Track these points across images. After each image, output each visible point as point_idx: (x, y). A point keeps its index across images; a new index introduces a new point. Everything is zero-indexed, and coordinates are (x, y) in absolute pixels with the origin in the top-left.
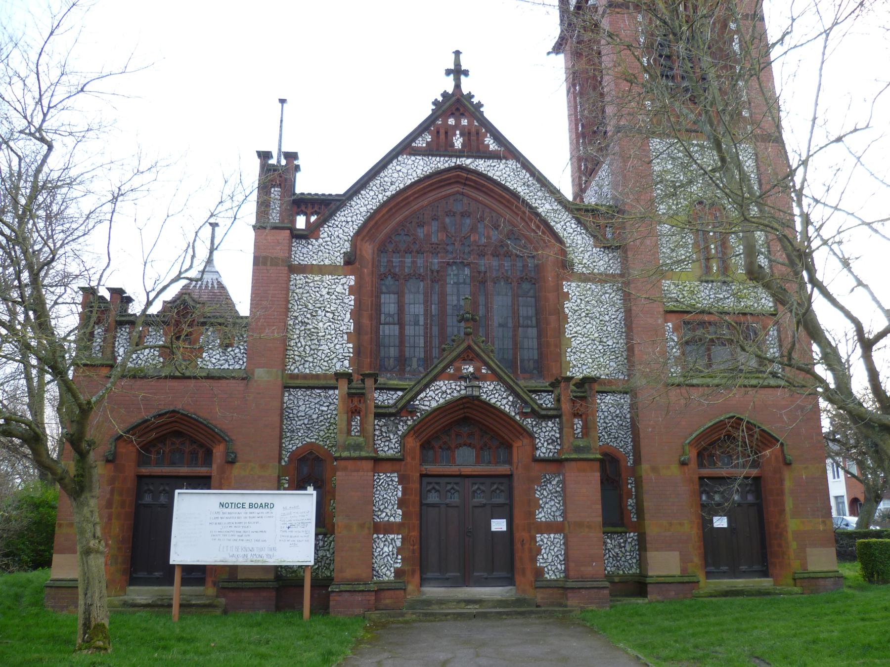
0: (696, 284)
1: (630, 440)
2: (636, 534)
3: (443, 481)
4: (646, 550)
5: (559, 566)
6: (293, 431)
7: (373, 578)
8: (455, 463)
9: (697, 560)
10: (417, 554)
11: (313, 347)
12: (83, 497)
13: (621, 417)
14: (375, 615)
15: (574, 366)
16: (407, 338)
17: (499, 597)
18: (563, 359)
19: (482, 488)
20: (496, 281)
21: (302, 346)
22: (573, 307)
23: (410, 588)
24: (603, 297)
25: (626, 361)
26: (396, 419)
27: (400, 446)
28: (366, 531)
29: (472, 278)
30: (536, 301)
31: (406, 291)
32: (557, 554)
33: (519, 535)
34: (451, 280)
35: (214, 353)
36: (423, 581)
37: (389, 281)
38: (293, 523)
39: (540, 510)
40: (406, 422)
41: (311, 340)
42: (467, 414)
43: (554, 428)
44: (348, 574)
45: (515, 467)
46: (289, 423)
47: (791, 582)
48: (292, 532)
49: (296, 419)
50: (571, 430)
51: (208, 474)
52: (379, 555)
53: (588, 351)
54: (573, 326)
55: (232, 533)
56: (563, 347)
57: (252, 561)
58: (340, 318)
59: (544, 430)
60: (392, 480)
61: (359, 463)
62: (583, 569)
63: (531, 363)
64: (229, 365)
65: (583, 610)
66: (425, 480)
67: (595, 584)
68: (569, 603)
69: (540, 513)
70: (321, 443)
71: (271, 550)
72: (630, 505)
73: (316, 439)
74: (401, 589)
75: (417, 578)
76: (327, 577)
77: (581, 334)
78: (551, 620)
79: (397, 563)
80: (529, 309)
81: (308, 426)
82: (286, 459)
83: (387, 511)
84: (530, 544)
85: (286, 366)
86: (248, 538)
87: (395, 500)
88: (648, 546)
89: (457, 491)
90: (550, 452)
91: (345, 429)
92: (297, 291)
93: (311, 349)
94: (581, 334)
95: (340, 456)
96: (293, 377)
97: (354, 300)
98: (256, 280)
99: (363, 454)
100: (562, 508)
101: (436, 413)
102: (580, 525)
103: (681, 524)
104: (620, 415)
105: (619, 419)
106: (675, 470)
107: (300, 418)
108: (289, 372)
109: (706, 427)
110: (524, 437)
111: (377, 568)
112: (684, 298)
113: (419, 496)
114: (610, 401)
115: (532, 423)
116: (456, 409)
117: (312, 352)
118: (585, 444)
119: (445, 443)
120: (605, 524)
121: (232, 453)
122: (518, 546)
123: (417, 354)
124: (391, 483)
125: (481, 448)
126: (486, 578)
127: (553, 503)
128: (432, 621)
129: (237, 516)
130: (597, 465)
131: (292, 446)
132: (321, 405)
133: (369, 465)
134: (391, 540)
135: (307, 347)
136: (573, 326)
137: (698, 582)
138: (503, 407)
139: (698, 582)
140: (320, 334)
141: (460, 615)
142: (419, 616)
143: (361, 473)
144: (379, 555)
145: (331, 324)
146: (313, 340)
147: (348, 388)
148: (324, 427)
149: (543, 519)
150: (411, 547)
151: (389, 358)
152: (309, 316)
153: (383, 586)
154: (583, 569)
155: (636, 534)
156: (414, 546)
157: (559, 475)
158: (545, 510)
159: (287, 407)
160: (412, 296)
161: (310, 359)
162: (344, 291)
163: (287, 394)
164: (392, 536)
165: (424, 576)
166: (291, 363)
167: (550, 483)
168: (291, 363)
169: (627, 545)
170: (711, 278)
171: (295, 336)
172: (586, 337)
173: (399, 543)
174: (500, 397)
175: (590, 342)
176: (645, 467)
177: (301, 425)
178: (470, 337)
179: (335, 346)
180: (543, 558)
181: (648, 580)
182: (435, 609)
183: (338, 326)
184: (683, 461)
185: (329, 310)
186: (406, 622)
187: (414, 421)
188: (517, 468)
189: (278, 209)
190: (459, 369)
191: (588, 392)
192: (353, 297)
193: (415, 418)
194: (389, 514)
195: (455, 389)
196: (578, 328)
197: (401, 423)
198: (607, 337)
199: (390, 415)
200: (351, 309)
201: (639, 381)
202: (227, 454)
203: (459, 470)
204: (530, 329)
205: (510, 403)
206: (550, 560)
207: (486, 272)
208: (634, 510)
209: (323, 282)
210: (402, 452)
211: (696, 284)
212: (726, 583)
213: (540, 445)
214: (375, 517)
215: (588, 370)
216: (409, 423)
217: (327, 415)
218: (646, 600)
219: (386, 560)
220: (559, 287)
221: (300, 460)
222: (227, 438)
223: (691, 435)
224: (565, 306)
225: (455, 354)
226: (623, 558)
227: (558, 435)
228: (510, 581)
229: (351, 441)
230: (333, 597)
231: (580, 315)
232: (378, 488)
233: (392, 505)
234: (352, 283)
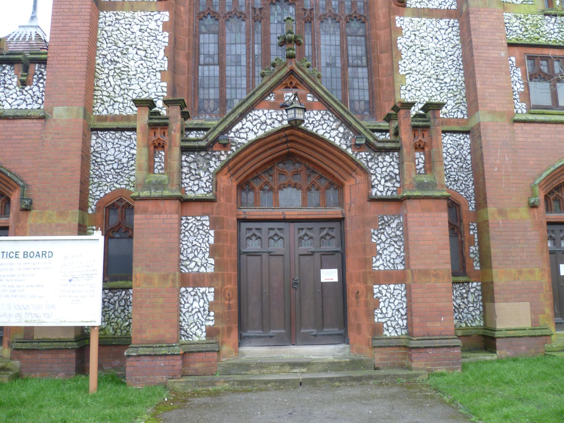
0: (539, 17)
1: (471, 183)
2: (480, 284)
3: (265, 226)
4: (493, 301)
5: (400, 322)
6: (101, 177)
7: (181, 338)
8: (278, 205)
9: (548, 311)
10: (235, 310)
11: (123, 87)
13: (461, 159)
14: (179, 384)
16: (228, 79)
17: (331, 358)
19: (310, 234)
20: (323, 19)
21: (111, 86)
22: (407, 43)
23: (225, 349)
24: (439, 33)
25: (465, 99)
26: (207, 154)
27: (212, 185)
28: (169, 284)
29: (297, 16)
30: (366, 40)
31: (227, 30)
32: (397, 307)
33: (351, 286)
34: (274, 19)
35: (11, 92)
36: (242, 340)
37: (209, 21)
39: (378, 257)
40: (219, 158)
41: (121, 80)
42: (291, 150)
43: (393, 163)
44: (149, 334)
45: (347, 209)
46: (97, 168)
49: (104, 163)
50: (412, 164)
51: (6, 225)
52: (188, 311)
53: (424, 88)
54: (407, 62)
57: (27, 322)
58: (152, 56)
59: (381, 165)
60: (203, 225)
61: (161, 204)
62: (429, 324)
63: (362, 103)
64: (27, 105)
65: (431, 374)
66: (244, 226)
67: (444, 343)
68: (414, 365)
69: (377, 260)
72: (473, 253)
73: (126, 185)
74: (214, 351)
75: (235, 335)
77: (416, 71)
78: (395, 390)
79: (209, 320)
80: (359, 48)
82: (93, 207)
83: (197, 260)
84: (366, 297)
85: (94, 107)
87: (205, 247)
88: (496, 296)
89: (282, 238)
90: (388, 190)
91: (145, 164)
92: (107, 28)
93: (121, 89)
94: (416, 71)
95: (139, 196)
96: (101, 118)
97: (169, 37)
98: (56, 7)
99: (166, 193)
100: (403, 254)
101: (254, 147)
102: (425, 273)
103: (531, 272)
104: (460, 156)
105: (459, 160)
106: (524, 213)
107: (109, 162)
108: (97, 114)
109: (557, 166)
110: (357, 174)
111: (186, 327)
112: (527, 31)
113: (236, 242)
114: (449, 142)
115: (366, 158)
116: (279, 142)
117: (122, 92)
118: (429, 179)
119: (267, 183)
120: (454, 274)
121: (27, 199)
122: (351, 299)
123: (239, 96)
124: (201, 227)
125: (309, 189)
126: (315, 336)
127: (392, 249)
128: (248, 391)
130: (444, 203)
132: (131, 148)
133: (175, 205)
135: (116, 87)
136: (407, 62)
137: (550, 335)
138: (332, 139)
139: (550, 335)
140: (131, 73)
141: (283, 382)
142: (233, 385)
143: (164, 216)
144: (188, 311)
145: (143, 62)
146: (124, 79)
147: (150, 119)
148: (134, 172)
149: (382, 268)
150: (227, 302)
151: (209, 100)
152: (119, 54)
153: (193, 348)
154: (429, 324)
155: (480, 284)
156: (230, 300)
157: (399, 217)
158: (383, 256)
159: (94, 151)
160: (233, 36)
161: (120, 99)
162: (157, 28)
163: (94, 137)
164: (202, 290)
165: (244, 334)
166: (99, 104)
167: (389, 225)
168: (99, 104)
169: (470, 296)
170: (553, 12)
171: (104, 76)
172: (422, 75)
173: (211, 298)
174: (329, 128)
175: (426, 79)
176: (491, 209)
177: (110, 170)
178: (293, 60)
179: (147, 85)
180: (382, 313)
181: (497, 334)
182: (255, 375)
183: (150, 64)
184: (533, 203)
185: (141, 47)
186: (217, 394)
187: (228, 155)
188: (349, 210)
190: (281, 97)
191: (432, 121)
192: (167, 34)
193: (229, 152)
194: (199, 264)
195: (276, 119)
196: (413, 65)
197: (214, 159)
199: (200, 149)
200: (165, 47)
201: (483, 117)
202: (22, 199)
203: (283, 214)
204: (360, 70)
205: (340, 135)
206: (390, 315)
207: (312, 9)
208: (477, 258)
209: (134, 18)
210: (214, 191)
211: (539, 17)
213: (376, 182)
214: (182, 267)
216: (223, 158)
218: (495, 357)
219: (196, 317)
221: (108, 208)
222: (21, 184)
223: (540, 175)
224: (398, 41)
225: (275, 79)
226: (466, 310)
227: (397, 171)
228: (343, 338)
229: (152, 178)
230: (129, 363)
231: (414, 51)
232: (187, 233)
233: (203, 253)
234: (167, 19)
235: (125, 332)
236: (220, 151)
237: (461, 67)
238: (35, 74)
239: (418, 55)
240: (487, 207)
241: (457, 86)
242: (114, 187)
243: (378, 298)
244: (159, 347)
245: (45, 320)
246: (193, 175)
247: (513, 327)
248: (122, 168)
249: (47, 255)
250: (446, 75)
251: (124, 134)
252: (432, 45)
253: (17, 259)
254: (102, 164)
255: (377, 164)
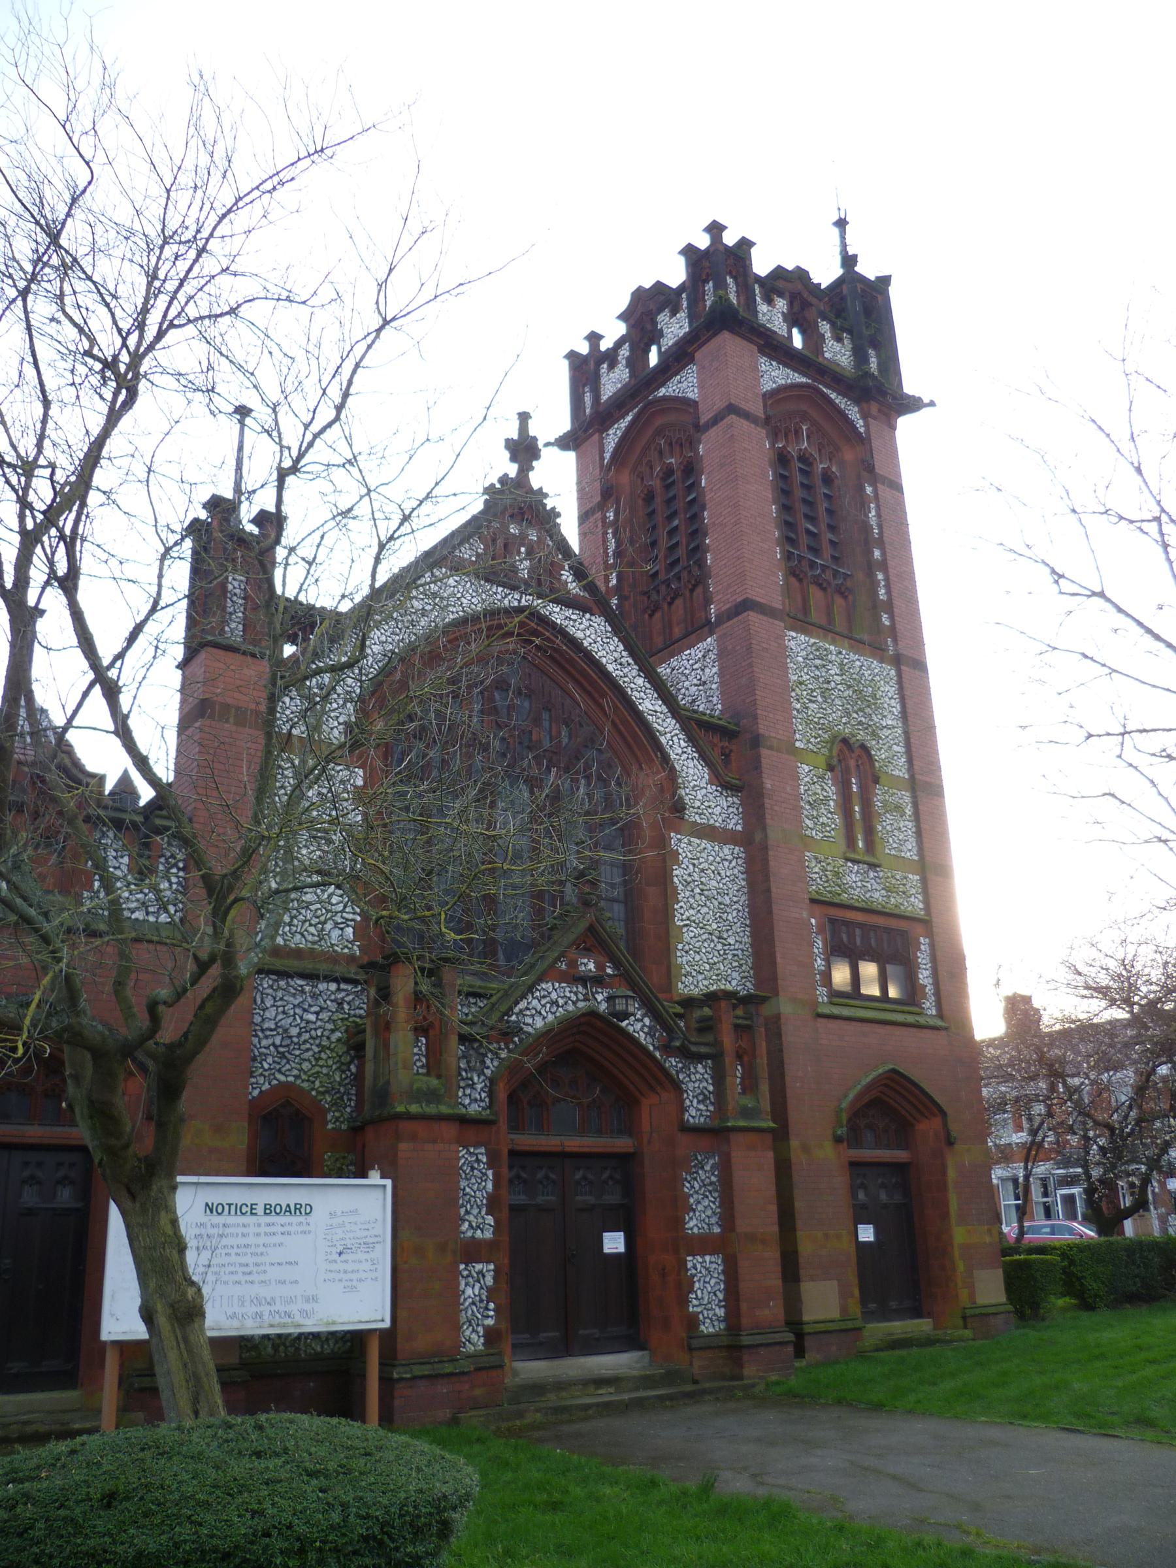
5: (717, 1310)
12: (154, 1187)
15: (688, 974)
18: (673, 961)
38: (349, 1243)
39: (691, 1214)
47: (960, 1322)
48: (346, 1261)
49: (260, 1034)
55: (232, 1269)
56: (672, 941)
57: (272, 1326)
60: (478, 1161)
69: (691, 1219)
70: (305, 1085)
71: (307, 1300)
73: (296, 1077)
76: (316, 1354)
79: (488, 1317)
81: (281, 1049)
83: (471, 1218)
86: (262, 1277)
87: (481, 1198)
88: (802, 1272)
90: (701, 1115)
107: (268, 1033)
127: (706, 1203)
129: (240, 1230)
131: (260, 1085)
134: (478, 1273)
141: (607, 1405)
148: (310, 1053)
149: (695, 1230)
164: (479, 1267)
167: (702, 1168)
173: (489, 1280)
177: (267, 1048)
188: (649, 1142)
189: (240, 615)
190: (573, 964)
196: (692, 912)
198: (727, 931)
205: (646, 1030)
206: (705, 1302)
212: (899, 1327)
215: (706, 983)
216: (504, 1054)
217: (316, 1029)
219: (470, 1312)
220: (661, 842)
228: (633, 1342)
233: (478, 1206)
235: (292, 1350)
236: (498, 1042)
237: (748, 922)
238: (163, 856)
239: (698, 897)
240: (788, 1139)
241: (743, 950)
242: (275, 1078)
243: (693, 1276)
244: (440, 1362)
245: (302, 1322)
246: (463, 1079)
247: (821, 1317)
248: (288, 1046)
249: (303, 1210)
250: (730, 933)
251: (292, 983)
252: (714, 883)
253: (254, 1218)
254: (256, 1036)
255: (689, 1076)
